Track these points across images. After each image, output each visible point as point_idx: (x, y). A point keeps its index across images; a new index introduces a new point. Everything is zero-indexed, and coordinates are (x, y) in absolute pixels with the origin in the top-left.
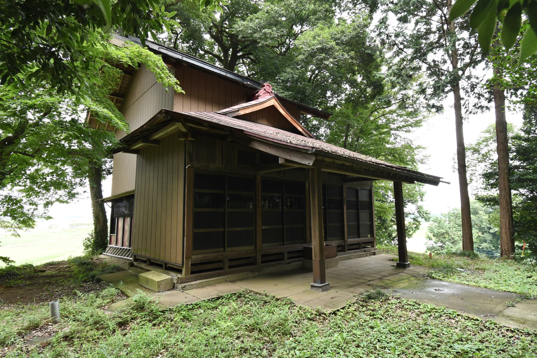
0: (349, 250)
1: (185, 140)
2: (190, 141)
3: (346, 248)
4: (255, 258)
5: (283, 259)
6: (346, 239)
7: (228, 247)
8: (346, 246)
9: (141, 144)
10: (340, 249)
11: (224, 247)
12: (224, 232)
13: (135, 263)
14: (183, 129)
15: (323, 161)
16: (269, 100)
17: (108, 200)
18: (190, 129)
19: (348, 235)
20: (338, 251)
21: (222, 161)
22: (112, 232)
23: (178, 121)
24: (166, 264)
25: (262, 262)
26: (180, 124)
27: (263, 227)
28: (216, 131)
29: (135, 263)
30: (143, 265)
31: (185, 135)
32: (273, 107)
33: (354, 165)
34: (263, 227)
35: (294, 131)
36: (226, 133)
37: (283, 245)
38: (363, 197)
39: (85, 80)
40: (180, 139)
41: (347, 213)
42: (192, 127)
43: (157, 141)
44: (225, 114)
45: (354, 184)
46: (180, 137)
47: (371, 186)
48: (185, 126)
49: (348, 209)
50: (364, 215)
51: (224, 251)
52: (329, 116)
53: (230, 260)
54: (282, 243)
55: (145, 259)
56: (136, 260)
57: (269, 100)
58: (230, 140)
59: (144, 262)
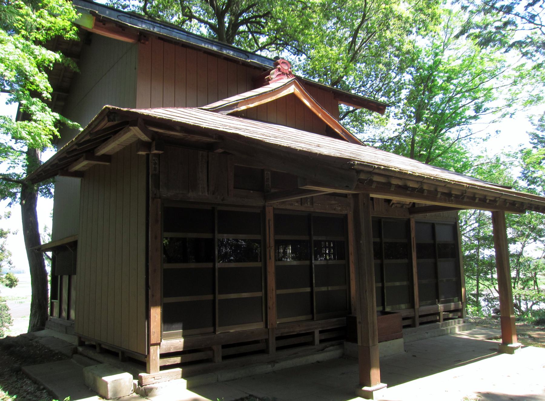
0: (421, 324)
1: (148, 155)
2: (155, 154)
3: (418, 321)
4: (267, 341)
5: (312, 343)
6: (417, 306)
7: (220, 326)
8: (417, 316)
9: (85, 163)
10: (407, 322)
11: (214, 325)
12: (214, 301)
13: (80, 349)
14: (144, 138)
15: (371, 182)
16: (285, 86)
17: (47, 247)
18: (154, 136)
19: (421, 300)
20: (405, 327)
21: (208, 186)
22: (54, 296)
23: (134, 124)
24: (123, 353)
25: (278, 349)
26: (137, 128)
27: (279, 292)
28: (197, 138)
29: (80, 349)
30: (91, 353)
31: (146, 146)
32: (293, 96)
33: (425, 187)
34: (279, 292)
35: (329, 132)
36: (213, 140)
37: (313, 319)
38: (443, 236)
39: (378, 80)
40: (140, 153)
41: (418, 264)
42: (157, 132)
43: (106, 158)
44: (216, 110)
45: (429, 217)
46: (138, 151)
47: (457, 218)
48: (144, 130)
49: (418, 258)
50: (445, 265)
51: (214, 332)
52: (385, 109)
53: (224, 347)
54: (310, 317)
55: (94, 344)
56: (82, 343)
57: (285, 86)
58: (220, 151)
59: (93, 347)
